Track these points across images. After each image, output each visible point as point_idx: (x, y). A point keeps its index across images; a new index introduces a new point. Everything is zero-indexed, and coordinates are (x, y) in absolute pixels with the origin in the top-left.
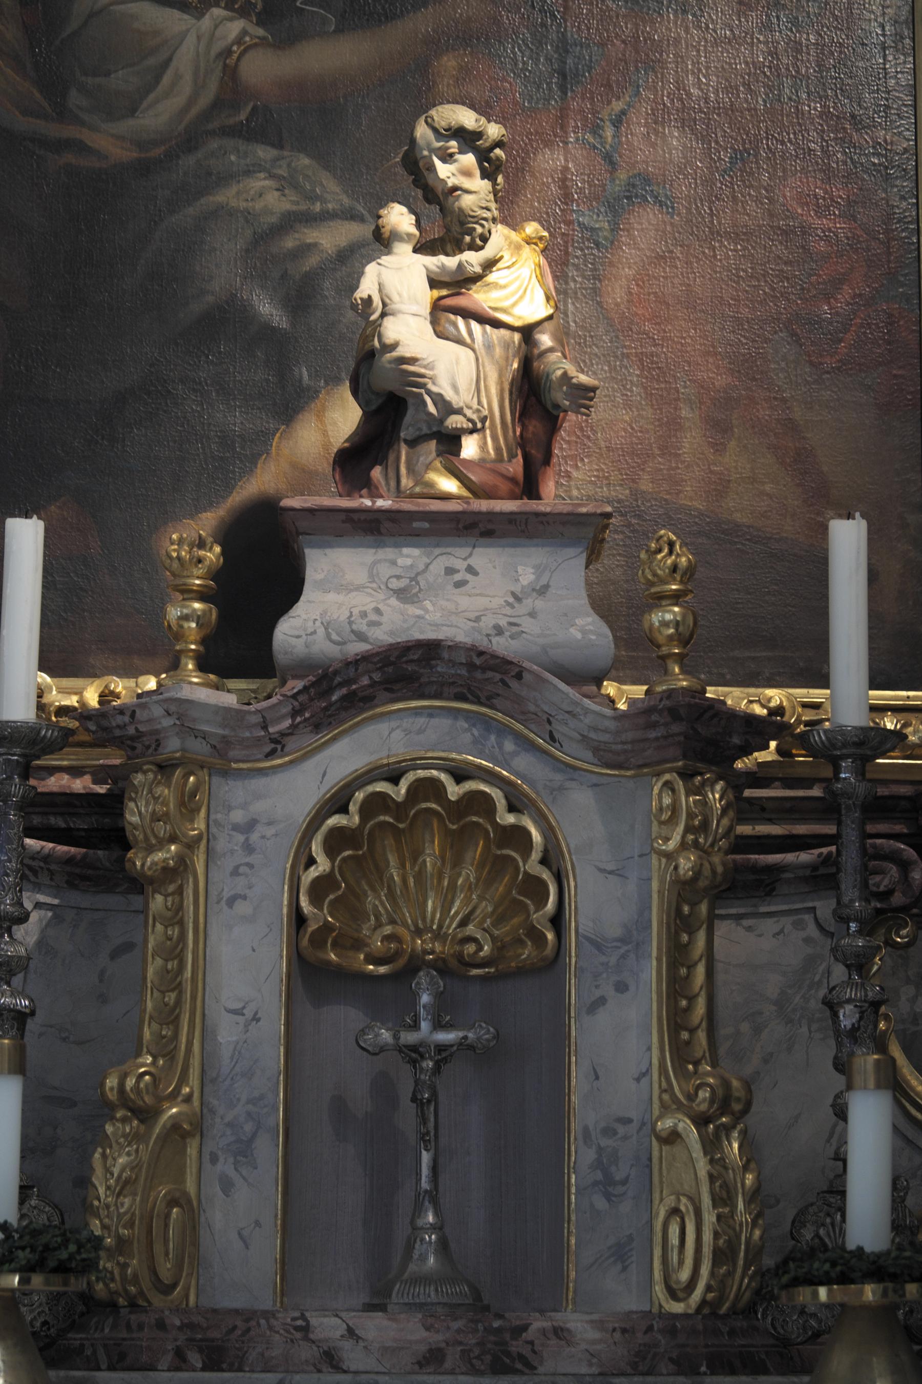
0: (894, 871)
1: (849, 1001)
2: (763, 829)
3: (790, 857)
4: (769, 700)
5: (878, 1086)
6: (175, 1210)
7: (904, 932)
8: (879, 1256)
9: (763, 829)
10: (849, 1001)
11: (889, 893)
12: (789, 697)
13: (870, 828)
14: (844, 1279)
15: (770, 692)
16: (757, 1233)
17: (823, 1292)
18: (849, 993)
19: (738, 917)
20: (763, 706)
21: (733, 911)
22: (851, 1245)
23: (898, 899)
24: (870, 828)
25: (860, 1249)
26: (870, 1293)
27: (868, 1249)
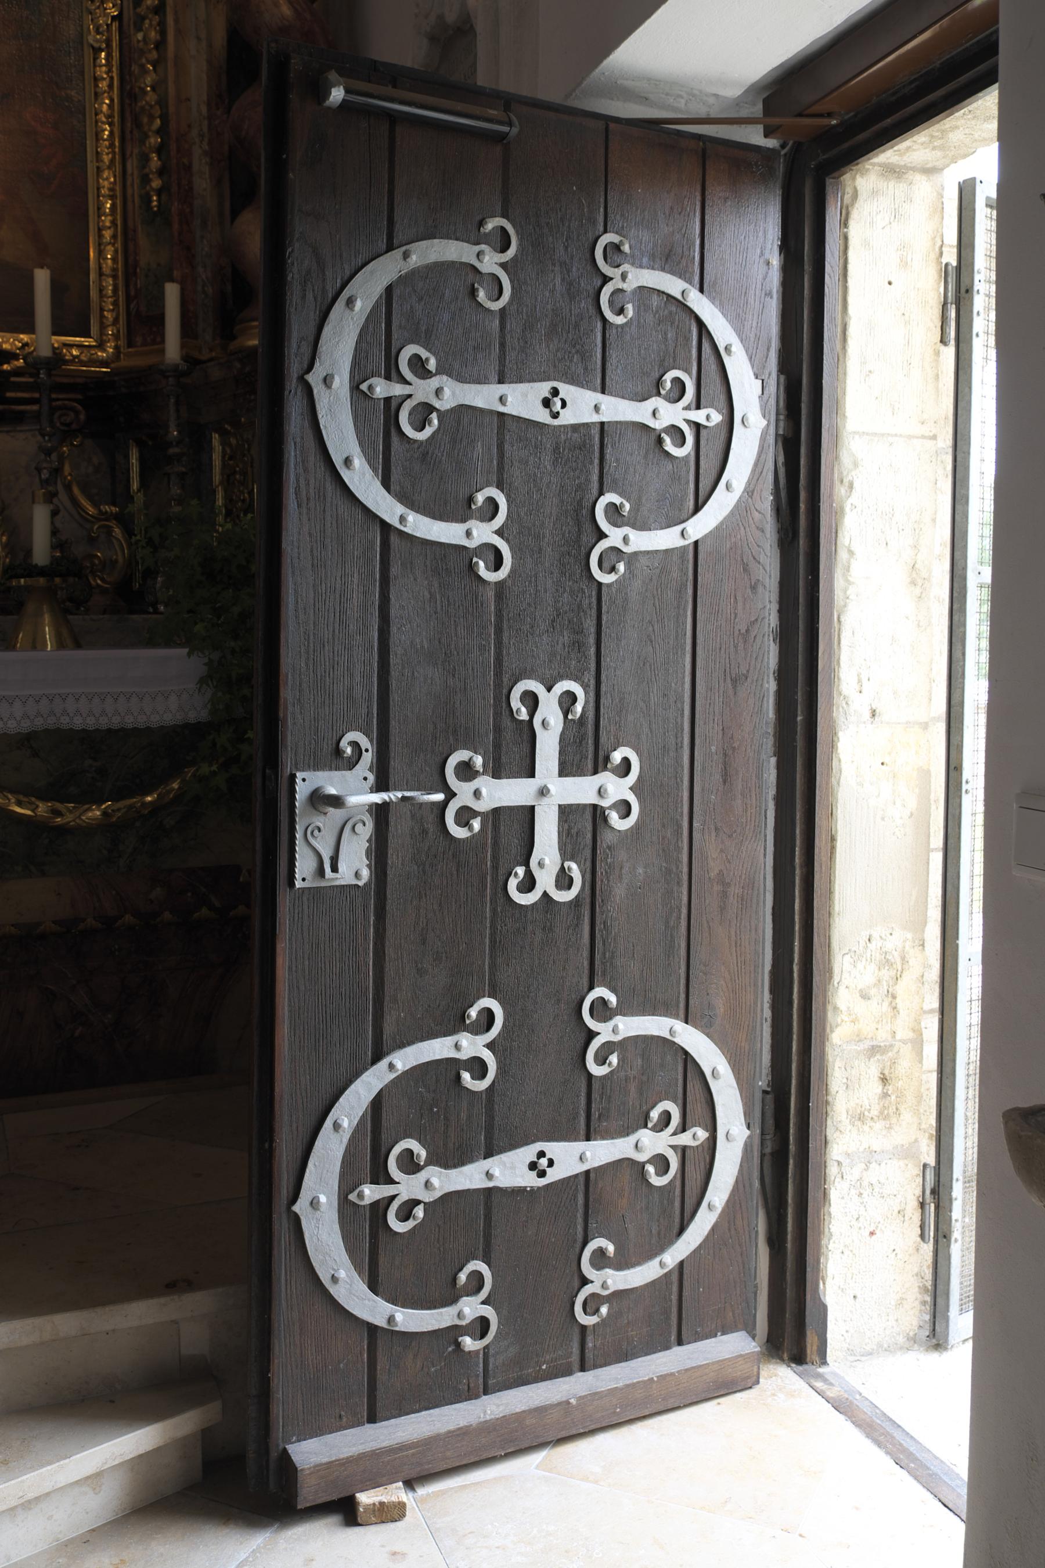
0: (72, 415)
1: (45, 468)
2: (20, 395)
3: (28, 408)
4: (22, 339)
5: (45, 502)
6: (1014, 873)
7: (78, 440)
8: (42, 567)
9: (20, 395)
10: (45, 468)
11: (71, 424)
12: (31, 339)
13: (54, 396)
14: (29, 575)
15: (22, 336)
16: (8, 560)
17: (22, 581)
18: (45, 465)
19: (8, 432)
20: (19, 342)
21: (5, 429)
22: (34, 563)
23: (74, 426)
24: (54, 396)
25: (36, 565)
26: (42, 581)
27: (39, 564)
